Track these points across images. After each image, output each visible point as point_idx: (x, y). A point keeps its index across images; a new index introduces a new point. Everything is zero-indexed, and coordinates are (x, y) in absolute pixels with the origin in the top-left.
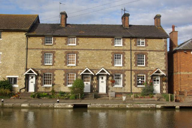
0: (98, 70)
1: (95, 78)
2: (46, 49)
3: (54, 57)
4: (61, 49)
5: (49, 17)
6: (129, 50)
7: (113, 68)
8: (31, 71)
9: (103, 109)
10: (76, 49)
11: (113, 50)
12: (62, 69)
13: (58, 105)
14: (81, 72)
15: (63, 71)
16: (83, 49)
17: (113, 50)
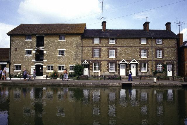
0: (120, 60)
1: (118, 66)
2: (95, 47)
3: (100, 52)
4: (105, 47)
5: (94, 25)
6: (82, 48)
7: (140, 59)
8: (123, 61)
9: (170, 87)
10: (115, 47)
11: (140, 47)
12: (106, 60)
13: (115, 84)
14: (119, 62)
15: (107, 61)
16: (120, 47)
17: (140, 47)
